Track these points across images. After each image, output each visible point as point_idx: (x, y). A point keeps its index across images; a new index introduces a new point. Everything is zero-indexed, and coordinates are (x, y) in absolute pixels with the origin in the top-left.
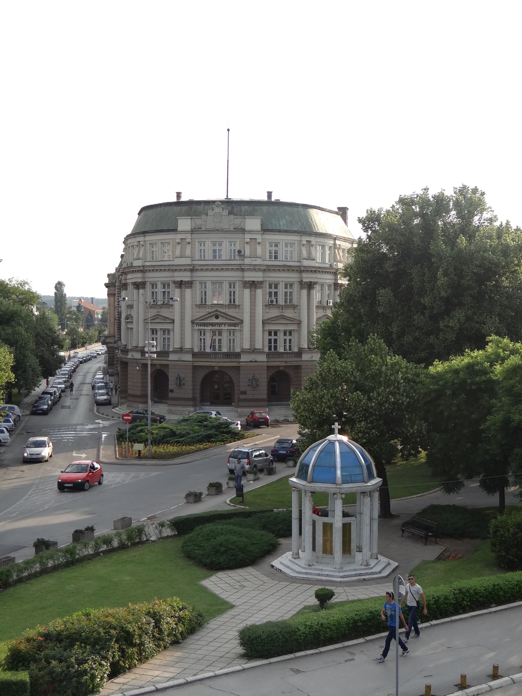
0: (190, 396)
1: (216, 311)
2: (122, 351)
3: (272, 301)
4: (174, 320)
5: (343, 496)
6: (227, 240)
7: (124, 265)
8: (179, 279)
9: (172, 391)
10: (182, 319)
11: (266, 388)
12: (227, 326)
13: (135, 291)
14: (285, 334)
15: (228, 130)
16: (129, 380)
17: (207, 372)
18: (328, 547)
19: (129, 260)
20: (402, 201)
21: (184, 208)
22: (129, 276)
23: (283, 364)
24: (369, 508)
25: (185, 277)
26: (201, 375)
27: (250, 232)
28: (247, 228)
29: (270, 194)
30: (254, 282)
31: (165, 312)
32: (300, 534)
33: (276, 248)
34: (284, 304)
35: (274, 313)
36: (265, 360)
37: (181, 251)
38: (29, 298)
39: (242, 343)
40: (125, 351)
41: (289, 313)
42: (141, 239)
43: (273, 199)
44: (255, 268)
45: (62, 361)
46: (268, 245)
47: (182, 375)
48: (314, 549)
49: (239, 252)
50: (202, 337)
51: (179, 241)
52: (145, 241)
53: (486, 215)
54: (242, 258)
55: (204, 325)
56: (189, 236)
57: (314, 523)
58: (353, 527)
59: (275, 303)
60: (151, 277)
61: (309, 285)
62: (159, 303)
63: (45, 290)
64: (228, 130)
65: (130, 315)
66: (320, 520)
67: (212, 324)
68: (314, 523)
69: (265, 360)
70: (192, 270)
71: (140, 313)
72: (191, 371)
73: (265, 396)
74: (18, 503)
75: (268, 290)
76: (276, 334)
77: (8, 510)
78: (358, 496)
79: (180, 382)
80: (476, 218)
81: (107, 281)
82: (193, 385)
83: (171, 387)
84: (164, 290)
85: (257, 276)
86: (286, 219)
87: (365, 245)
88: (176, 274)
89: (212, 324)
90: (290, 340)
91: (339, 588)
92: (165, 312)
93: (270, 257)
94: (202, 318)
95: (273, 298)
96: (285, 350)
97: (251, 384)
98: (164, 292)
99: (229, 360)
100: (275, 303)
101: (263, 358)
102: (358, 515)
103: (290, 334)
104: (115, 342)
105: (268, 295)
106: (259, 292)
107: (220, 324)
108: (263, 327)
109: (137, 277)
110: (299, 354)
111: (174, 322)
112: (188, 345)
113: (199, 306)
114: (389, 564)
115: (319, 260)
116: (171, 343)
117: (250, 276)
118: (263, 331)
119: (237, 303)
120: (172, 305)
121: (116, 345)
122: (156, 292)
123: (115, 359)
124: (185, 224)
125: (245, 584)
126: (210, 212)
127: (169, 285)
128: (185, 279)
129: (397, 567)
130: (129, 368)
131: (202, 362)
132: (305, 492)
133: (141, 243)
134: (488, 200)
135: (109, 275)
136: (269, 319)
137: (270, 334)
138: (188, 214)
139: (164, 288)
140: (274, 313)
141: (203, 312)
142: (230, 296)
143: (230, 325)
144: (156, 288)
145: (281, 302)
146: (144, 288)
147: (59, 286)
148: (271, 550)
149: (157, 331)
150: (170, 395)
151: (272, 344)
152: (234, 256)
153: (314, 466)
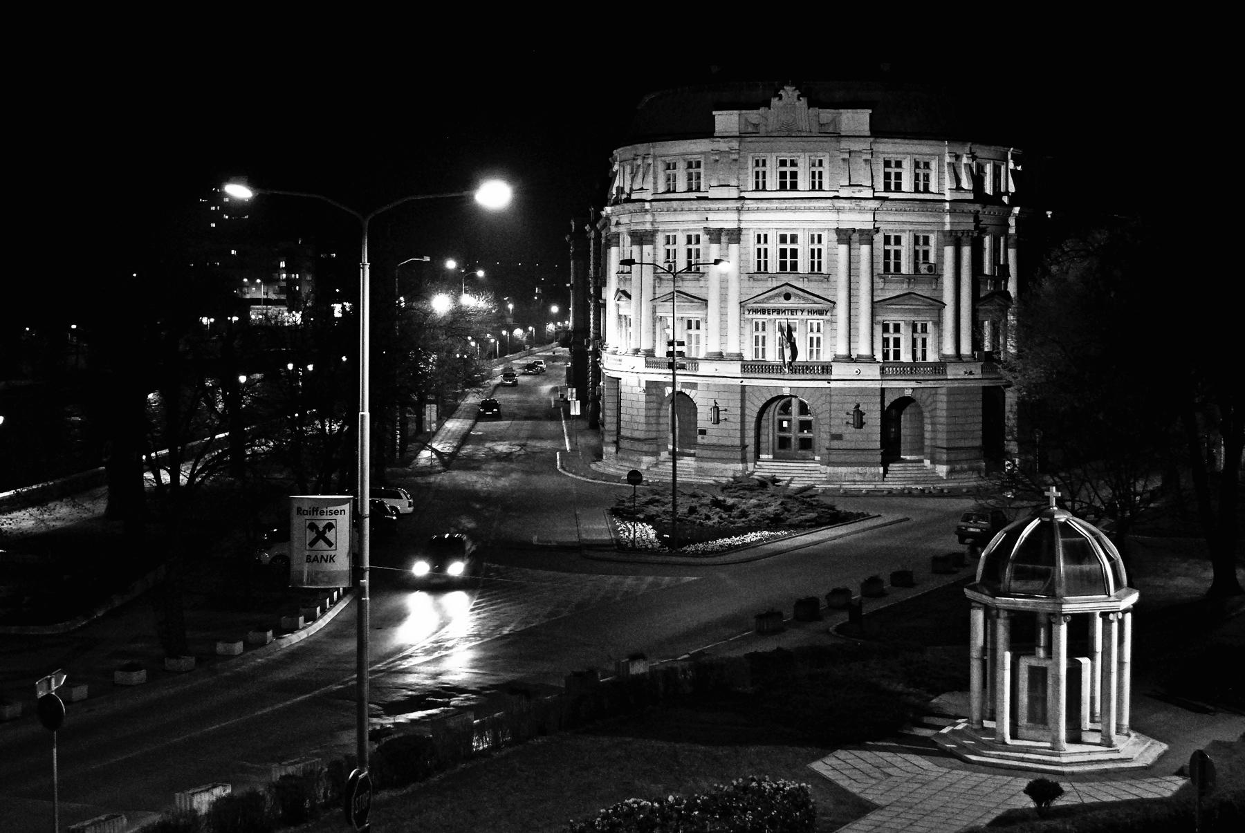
5: (1069, 618)
12: (805, 313)
31: (689, 286)
50: (760, 334)
67: (779, 311)
82: (743, 422)
89: (779, 311)
92: (689, 286)
101: (873, 371)
107: (793, 311)
108: (873, 316)
112: (732, 348)
118: (873, 322)
119: (824, 270)
125: (890, 770)
127: (698, 238)
137: (886, 328)
141: (759, 288)
142: (759, 256)
146: (652, 242)
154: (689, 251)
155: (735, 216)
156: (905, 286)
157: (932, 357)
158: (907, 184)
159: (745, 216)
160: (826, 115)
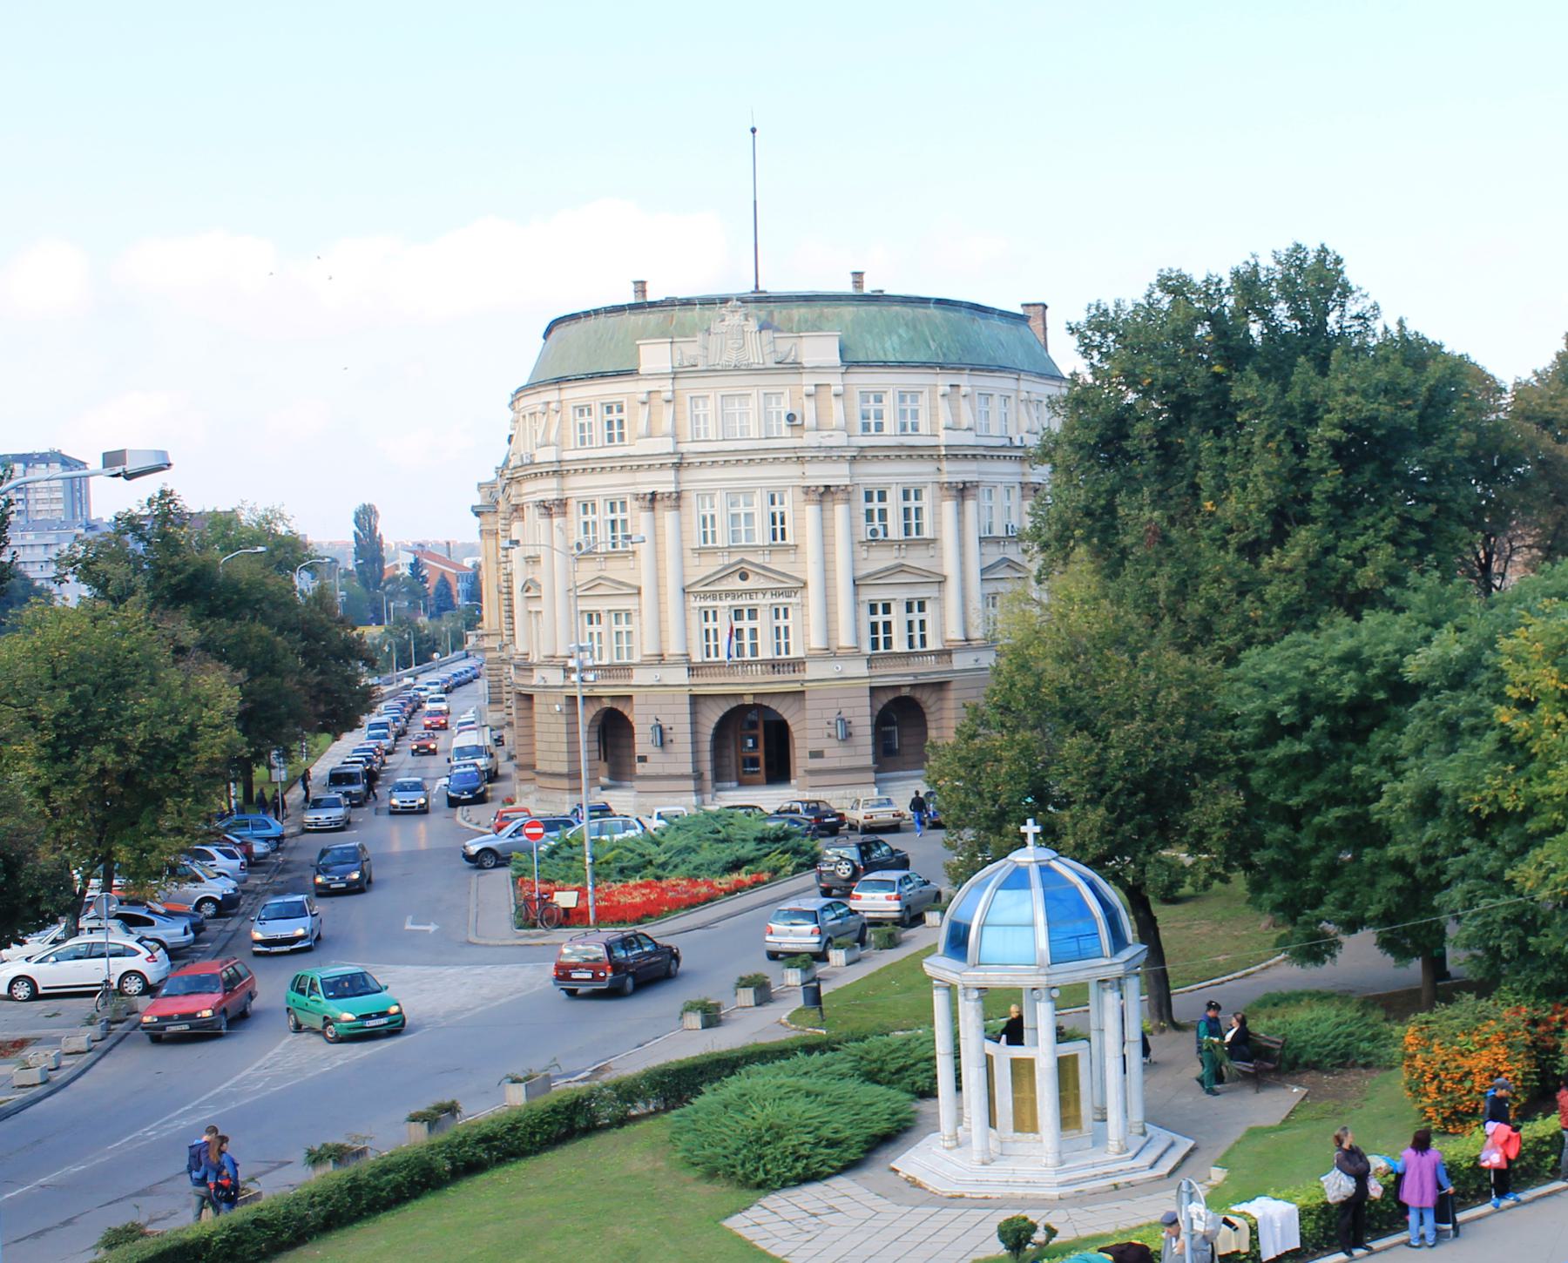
0: (564, 769)
1: (742, 561)
2: (517, 667)
3: (874, 532)
4: (639, 589)
5: (1056, 993)
6: (762, 391)
7: (515, 462)
8: (959, 478)
9: (643, 759)
10: (658, 585)
11: (869, 740)
12: (768, 595)
13: (544, 522)
14: (909, 609)
15: (753, 131)
16: (538, 737)
17: (727, 708)
18: (1027, 1117)
19: (525, 447)
20: (1164, 284)
21: (653, 318)
22: (528, 487)
23: (910, 680)
24: (1117, 1018)
25: (663, 482)
26: (712, 717)
27: (815, 369)
28: (807, 361)
29: (641, 286)
30: (827, 487)
31: (617, 570)
32: (959, 1089)
33: (878, 406)
34: (902, 537)
35: (882, 559)
36: (864, 671)
37: (649, 421)
38: (289, 553)
39: (806, 635)
40: (526, 667)
41: (917, 558)
42: (552, 395)
43: (867, 290)
44: (828, 455)
45: (367, 700)
46: (857, 397)
47: (666, 722)
48: (992, 1123)
49: (791, 417)
51: (644, 397)
52: (560, 402)
53: (1353, 308)
54: (797, 432)
55: (714, 595)
56: (667, 385)
57: (989, 1061)
58: (1083, 1065)
59: (881, 536)
60: (578, 487)
61: (962, 490)
62: (601, 549)
63: (326, 530)
64: (753, 131)
65: (532, 580)
66: (1004, 1053)
67: (733, 594)
68: (989, 1061)
69: (864, 671)
70: (678, 466)
71: (555, 574)
72: (687, 709)
73: (868, 761)
74: (270, 1054)
75: (863, 506)
76: (887, 609)
77: (244, 1074)
78: (1093, 989)
79: (662, 738)
80: (1332, 319)
81: (477, 500)
83: (639, 750)
84: (613, 516)
85: (837, 474)
86: (900, 336)
87: (1087, 388)
88: (641, 476)
89: (733, 594)
90: (922, 623)
91: (1054, 1213)
92: (617, 570)
93: (866, 427)
94: (707, 580)
95: (876, 523)
96: (911, 646)
97: (833, 732)
98: (613, 522)
99: (777, 677)
100: (881, 536)
102: (1094, 1036)
103: (922, 608)
104: (502, 648)
105: (864, 518)
106: (840, 510)
107: (750, 593)
108: (856, 594)
109: (547, 489)
110: (945, 653)
111: (639, 593)
113: (700, 552)
114: (1172, 1144)
115: (924, 428)
116: (636, 644)
117: (821, 474)
118: (857, 604)
119: (927, 533)
120: (634, 552)
121: (504, 655)
122: (624, 521)
123: (505, 689)
124: (655, 356)
126: (717, 327)
128: (660, 489)
129: (1192, 1150)
130: (537, 708)
131: (711, 684)
132: (966, 988)
133: (553, 406)
134: (1352, 274)
135: (480, 486)
136: (869, 576)
137: (873, 609)
138: (668, 334)
139: (586, 513)
140: (882, 559)
141: (712, 565)
143: (776, 592)
144: (594, 512)
145: (895, 530)
147: (365, 517)
148: (894, 1134)
149: (599, 616)
150: (640, 768)
151: (880, 633)
152: (779, 427)
153: (982, 926)
154: (907, 511)
155: (670, 475)
156: (895, 553)
157: (932, 645)
158: (890, 426)
159: (687, 475)
160: (785, 345)
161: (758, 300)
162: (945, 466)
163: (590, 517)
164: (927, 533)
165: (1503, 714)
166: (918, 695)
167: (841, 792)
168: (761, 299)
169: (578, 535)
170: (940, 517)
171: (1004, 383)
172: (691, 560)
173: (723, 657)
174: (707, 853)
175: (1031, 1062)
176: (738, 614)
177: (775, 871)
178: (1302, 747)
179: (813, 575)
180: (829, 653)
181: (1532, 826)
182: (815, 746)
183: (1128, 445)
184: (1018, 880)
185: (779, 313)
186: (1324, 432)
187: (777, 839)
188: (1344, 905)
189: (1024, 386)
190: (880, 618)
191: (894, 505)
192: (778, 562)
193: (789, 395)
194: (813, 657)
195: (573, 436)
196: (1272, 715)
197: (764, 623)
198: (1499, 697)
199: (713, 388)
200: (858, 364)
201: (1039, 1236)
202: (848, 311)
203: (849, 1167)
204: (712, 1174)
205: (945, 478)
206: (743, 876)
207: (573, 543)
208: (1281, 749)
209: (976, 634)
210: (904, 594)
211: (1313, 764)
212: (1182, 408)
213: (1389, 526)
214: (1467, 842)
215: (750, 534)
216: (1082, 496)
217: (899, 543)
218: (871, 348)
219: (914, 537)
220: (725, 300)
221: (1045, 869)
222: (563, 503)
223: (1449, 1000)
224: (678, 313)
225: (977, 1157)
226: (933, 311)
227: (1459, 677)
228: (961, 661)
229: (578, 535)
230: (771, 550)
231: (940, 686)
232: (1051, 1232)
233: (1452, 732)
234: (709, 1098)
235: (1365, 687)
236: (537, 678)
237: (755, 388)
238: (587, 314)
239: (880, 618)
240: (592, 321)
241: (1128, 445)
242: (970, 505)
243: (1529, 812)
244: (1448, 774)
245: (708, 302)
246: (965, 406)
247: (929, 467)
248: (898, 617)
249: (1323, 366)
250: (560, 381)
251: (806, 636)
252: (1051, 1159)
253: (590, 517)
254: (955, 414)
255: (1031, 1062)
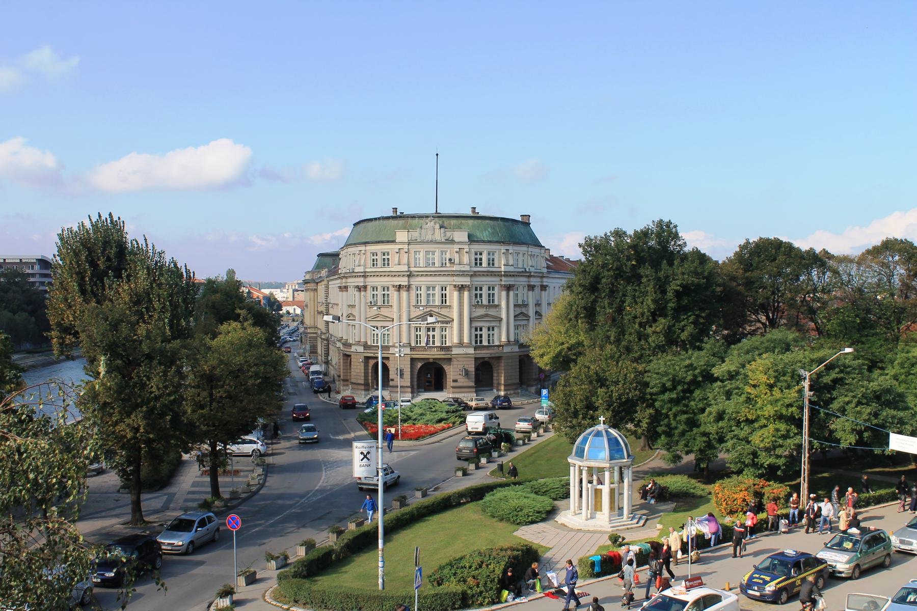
0: (362, 382)
9: (392, 380)
13: (357, 294)
14: (489, 330)
21: (401, 222)
22: (350, 280)
25: (404, 281)
27: (459, 243)
28: (456, 239)
29: (395, 210)
35: (480, 312)
39: (452, 338)
41: (492, 312)
42: (362, 248)
44: (463, 274)
49: (450, 260)
60: (371, 281)
70: (409, 276)
76: (481, 330)
85: (466, 281)
109: (360, 282)
116: (390, 338)
118: (471, 327)
119: (496, 303)
124: (402, 236)
126: (424, 226)
137: (476, 330)
138: (408, 228)
140: (480, 312)
143: (442, 322)
157: (497, 343)
158: (485, 264)
160: (449, 234)
161: (438, 217)
162: (503, 278)
163: (375, 293)
164: (496, 303)
165: (748, 389)
166: (491, 361)
167: (466, 395)
168: (438, 216)
169: (370, 299)
170: (502, 299)
171: (523, 249)
172: (412, 309)
173: (423, 344)
174: (428, 417)
175: (601, 490)
176: (428, 330)
177: (454, 423)
178: (674, 396)
179: (504, 316)
180: (461, 344)
181: (756, 425)
182: (455, 378)
183: (600, 286)
184: (598, 434)
185: (446, 222)
186: (674, 286)
187: (453, 412)
188: (686, 446)
189: (530, 249)
190: (479, 333)
191: (485, 292)
192: (444, 311)
193: (451, 252)
194: (455, 346)
195: (370, 263)
196: (664, 385)
197: (437, 333)
198: (747, 384)
199: (422, 249)
200: (474, 241)
201: (620, 540)
202: (471, 222)
203: (543, 520)
204: (502, 520)
205: (503, 283)
206: (442, 424)
207: (368, 301)
208: (666, 396)
209: (512, 339)
210: (487, 324)
211: (676, 402)
212: (619, 274)
213: (691, 319)
214: (734, 428)
215: (434, 301)
216: (582, 303)
217: (486, 306)
218: (480, 235)
219: (492, 305)
220: (427, 217)
221: (607, 432)
222: (365, 287)
223: (729, 477)
224: (410, 221)
225: (584, 518)
226: (500, 222)
227: (732, 376)
228: (507, 349)
229: (370, 299)
230: (441, 307)
231: (498, 358)
232: (624, 539)
233: (728, 395)
234: (488, 497)
235: (695, 376)
236: (353, 349)
237: (437, 249)
238: (375, 219)
239: (479, 333)
240: (377, 222)
241: (600, 286)
242: (511, 293)
243: (756, 420)
244: (730, 406)
245: (421, 217)
246: (510, 256)
247: (498, 279)
248: (485, 332)
249: (671, 264)
250: (366, 243)
251: (453, 338)
252: (607, 520)
253: (375, 293)
254: (507, 260)
255: (601, 490)
